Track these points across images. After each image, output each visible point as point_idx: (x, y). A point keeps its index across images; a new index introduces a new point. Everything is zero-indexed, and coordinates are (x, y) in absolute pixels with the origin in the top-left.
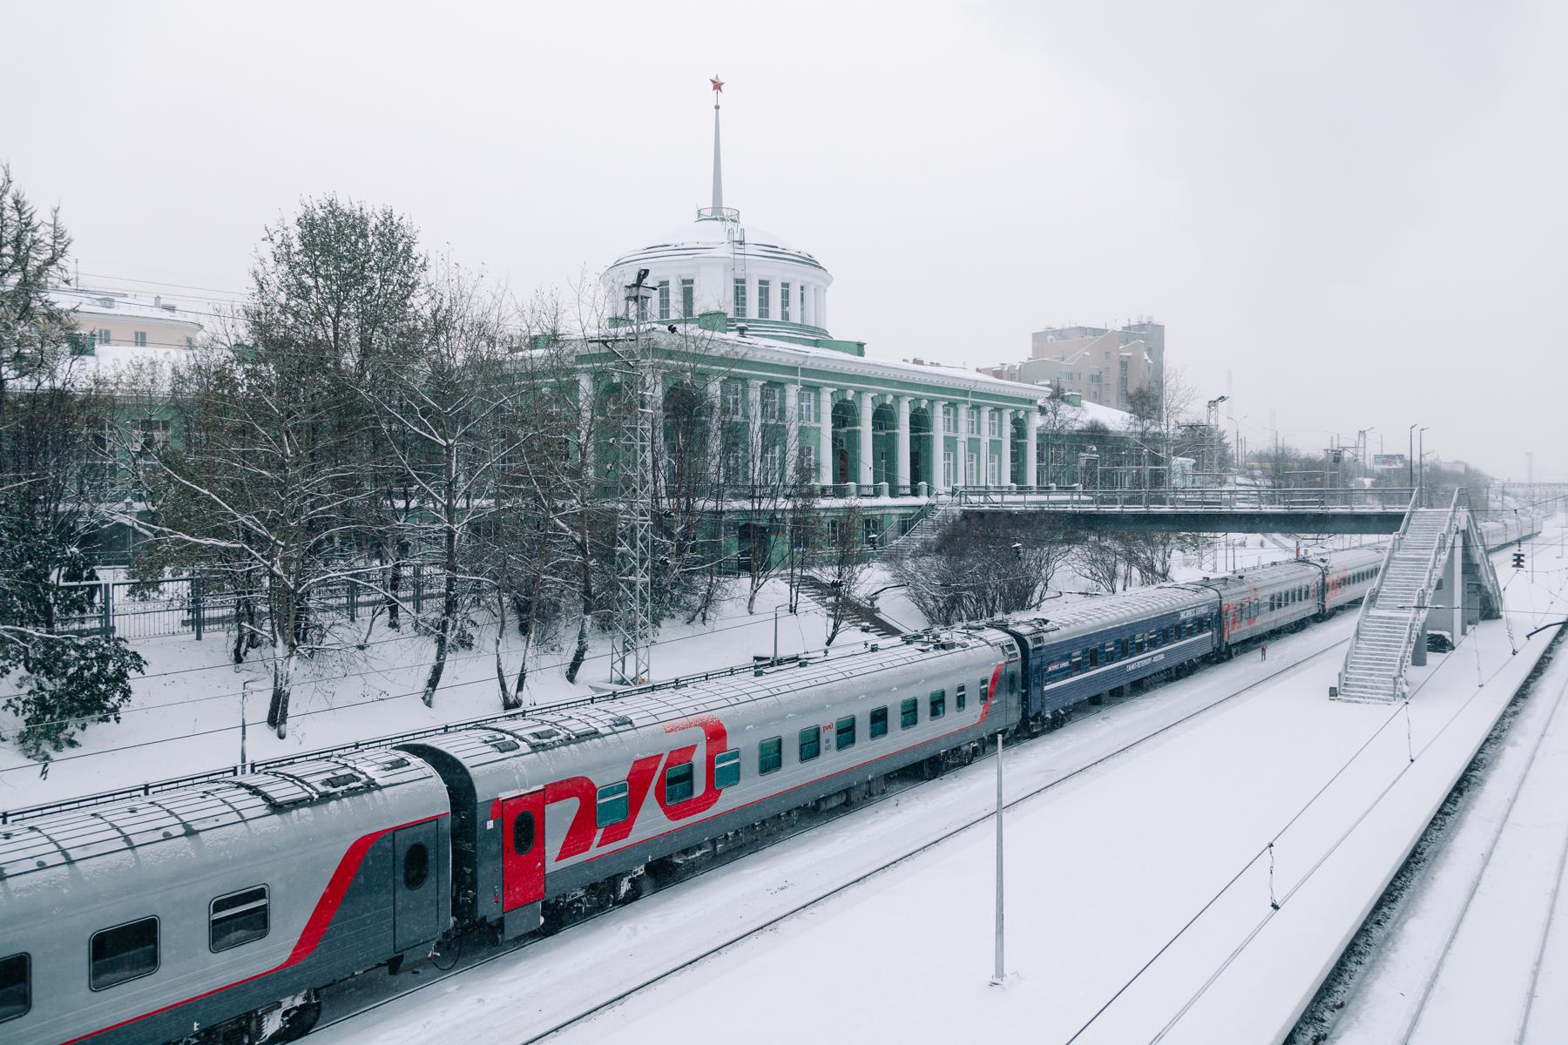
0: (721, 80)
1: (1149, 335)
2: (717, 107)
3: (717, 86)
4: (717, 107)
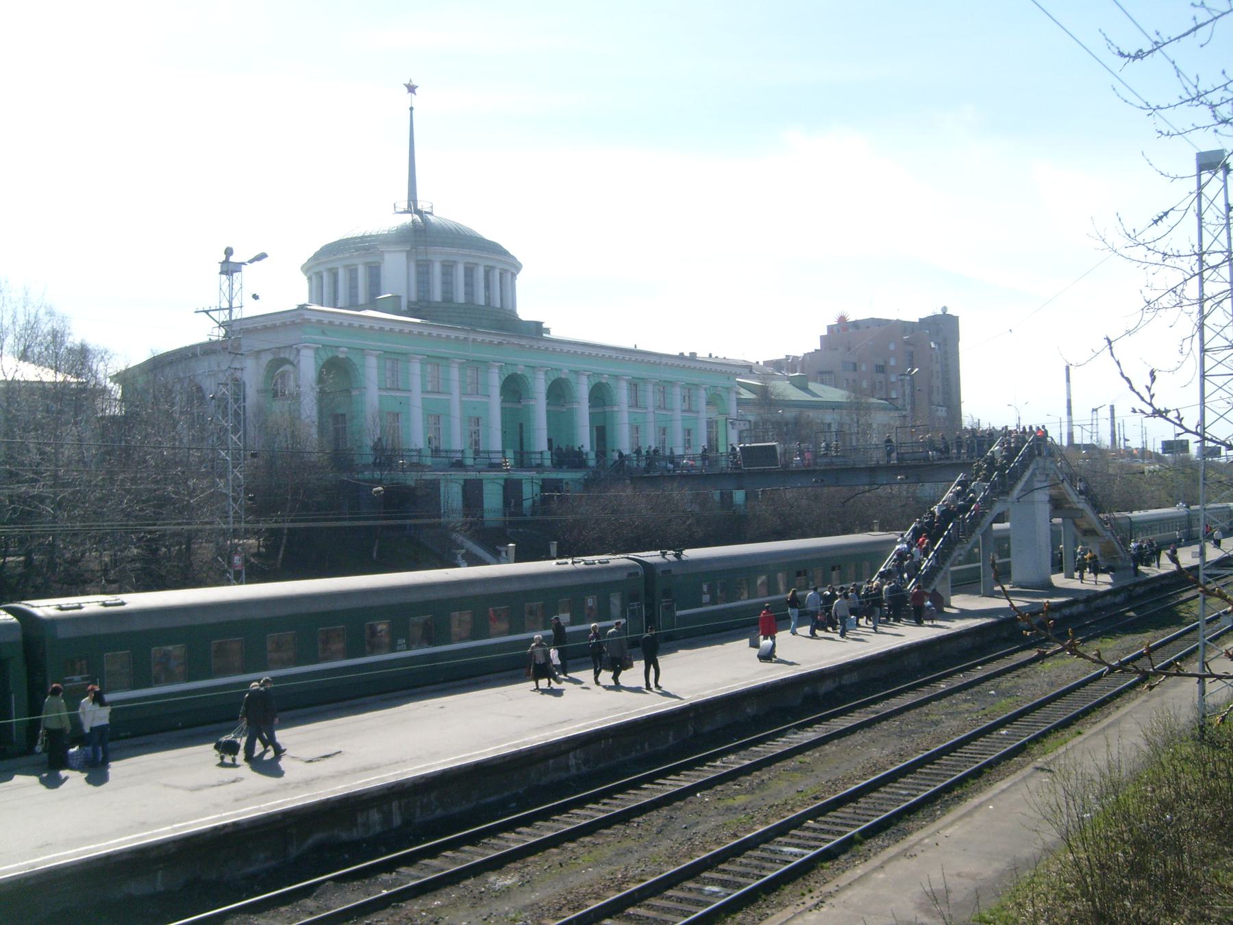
0: (414, 83)
1: (942, 330)
2: (411, 109)
3: (411, 89)
4: (411, 109)
